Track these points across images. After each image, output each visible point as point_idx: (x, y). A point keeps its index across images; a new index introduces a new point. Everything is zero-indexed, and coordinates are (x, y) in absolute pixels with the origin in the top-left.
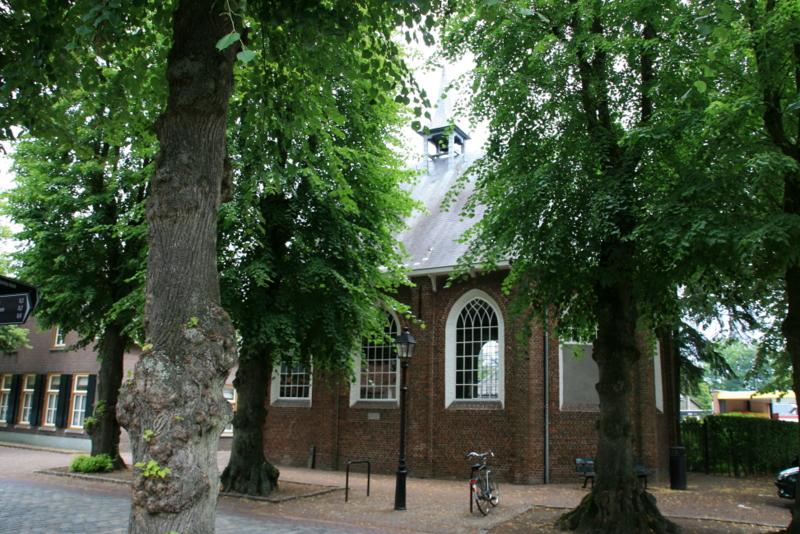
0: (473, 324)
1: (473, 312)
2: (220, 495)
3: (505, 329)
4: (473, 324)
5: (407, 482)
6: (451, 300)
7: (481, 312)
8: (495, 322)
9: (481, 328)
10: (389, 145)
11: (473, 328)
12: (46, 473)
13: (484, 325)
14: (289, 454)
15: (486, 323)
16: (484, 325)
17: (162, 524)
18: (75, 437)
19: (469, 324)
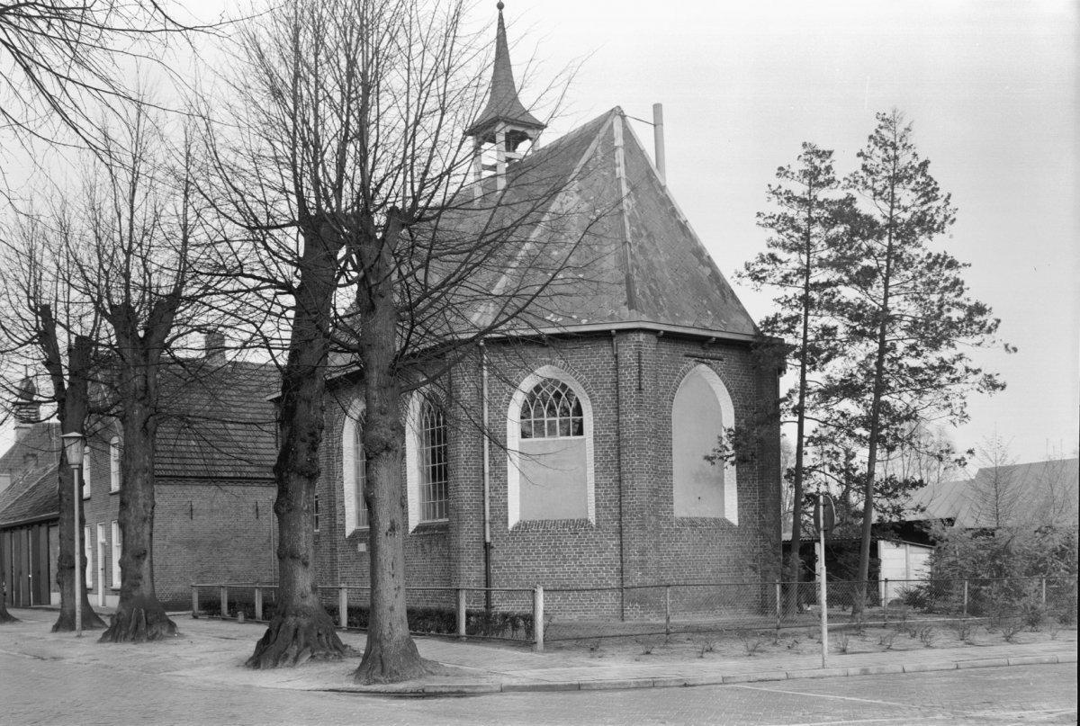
8: (578, 411)
13: (562, 415)
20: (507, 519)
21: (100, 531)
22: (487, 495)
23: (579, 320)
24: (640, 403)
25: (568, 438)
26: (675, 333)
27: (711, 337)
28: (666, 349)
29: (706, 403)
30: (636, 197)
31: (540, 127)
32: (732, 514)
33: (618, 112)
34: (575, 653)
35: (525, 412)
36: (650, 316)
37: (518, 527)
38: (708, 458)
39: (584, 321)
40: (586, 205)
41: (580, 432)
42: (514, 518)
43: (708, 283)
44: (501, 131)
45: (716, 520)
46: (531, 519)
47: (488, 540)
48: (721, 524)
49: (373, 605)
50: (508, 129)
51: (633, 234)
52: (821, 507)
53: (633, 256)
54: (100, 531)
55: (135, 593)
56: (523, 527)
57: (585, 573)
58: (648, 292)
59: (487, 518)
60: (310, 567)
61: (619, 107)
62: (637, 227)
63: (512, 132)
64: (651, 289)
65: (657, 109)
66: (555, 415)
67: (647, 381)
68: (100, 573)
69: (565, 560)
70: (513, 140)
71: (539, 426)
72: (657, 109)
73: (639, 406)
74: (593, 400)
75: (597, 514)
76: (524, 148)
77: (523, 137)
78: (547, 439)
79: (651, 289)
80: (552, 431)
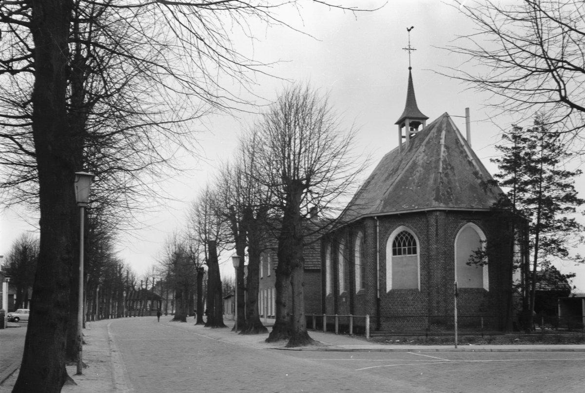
0: (397, 245)
1: (402, 238)
2: (89, 345)
3: (552, 344)
4: (397, 245)
5: (37, 236)
6: (387, 235)
7: (407, 238)
8: (415, 244)
9: (397, 248)
10: (189, 215)
11: (397, 248)
12: (489, 364)
13: (398, 247)
14: (162, 287)
15: (409, 245)
16: (398, 247)
17: (410, 32)
18: (563, 349)
19: (399, 245)
20: (386, 289)
21: (265, 291)
22: (378, 279)
23: (414, 207)
24: (437, 240)
25: (400, 256)
26: (461, 211)
27: (473, 211)
28: (451, 219)
29: (469, 240)
30: (448, 152)
31: (427, 118)
32: (486, 285)
33: (446, 116)
34: (371, 343)
35: (394, 245)
36: (444, 203)
37: (390, 292)
38: (468, 264)
39: (416, 207)
40: (426, 157)
41: (415, 252)
42: (389, 287)
43: (479, 187)
44: (407, 122)
45: (478, 289)
46: (396, 288)
47: (378, 296)
48: (481, 291)
49: (271, 326)
50: (411, 121)
51: (443, 169)
52: (378, 291)
53: (441, 178)
54: (265, 291)
55: (251, 316)
56: (392, 292)
57: (416, 311)
58: (446, 193)
59: (378, 288)
60: (286, 307)
61: (446, 113)
62: (446, 165)
63: (413, 122)
64: (447, 192)
65: (467, 110)
66: (406, 246)
67: (440, 232)
68: (265, 308)
69: (408, 305)
70: (415, 125)
71: (400, 250)
72: (467, 110)
73: (437, 242)
74: (419, 240)
75: (421, 287)
76: (420, 128)
77: (420, 124)
78: (402, 256)
79: (447, 192)
80: (405, 253)
